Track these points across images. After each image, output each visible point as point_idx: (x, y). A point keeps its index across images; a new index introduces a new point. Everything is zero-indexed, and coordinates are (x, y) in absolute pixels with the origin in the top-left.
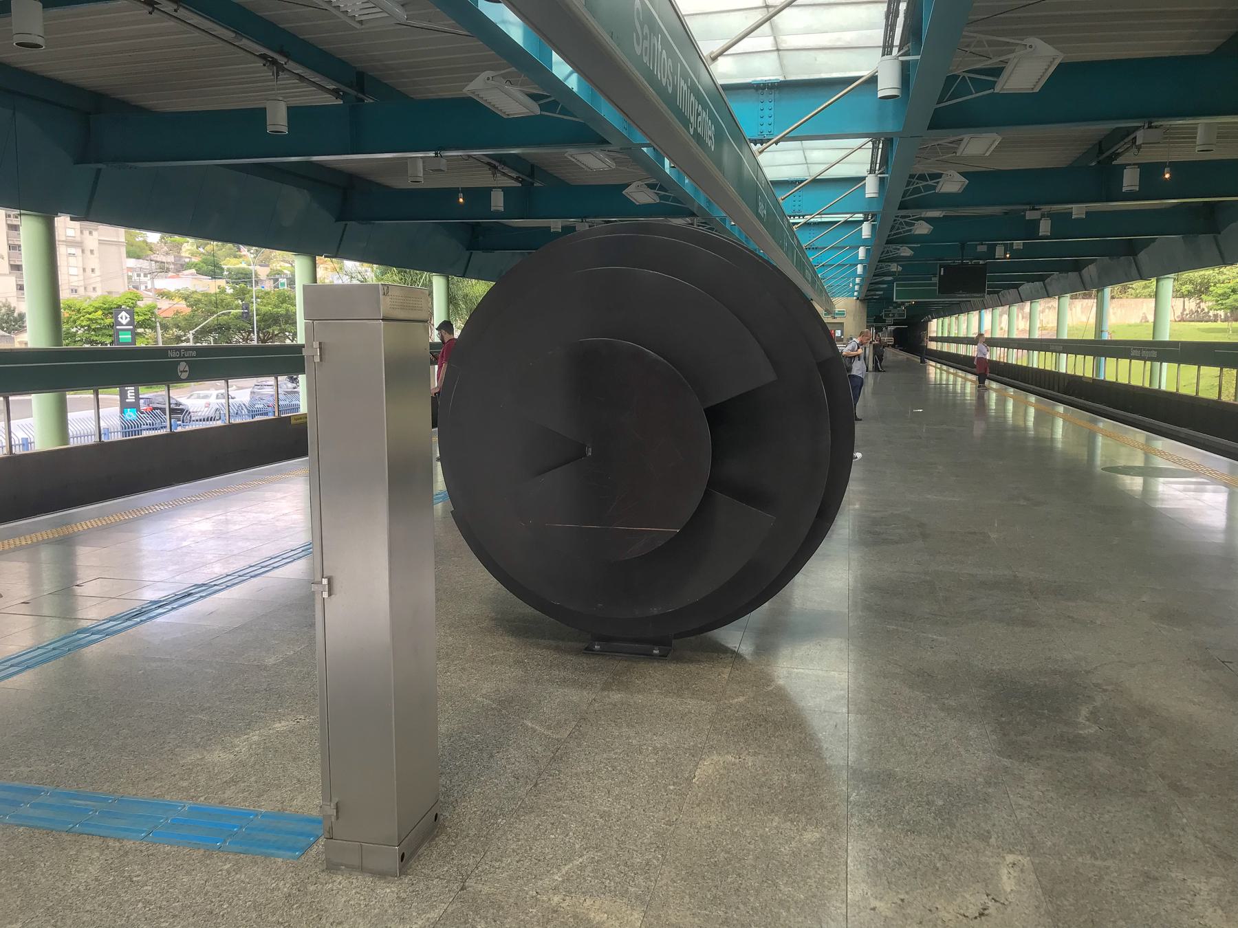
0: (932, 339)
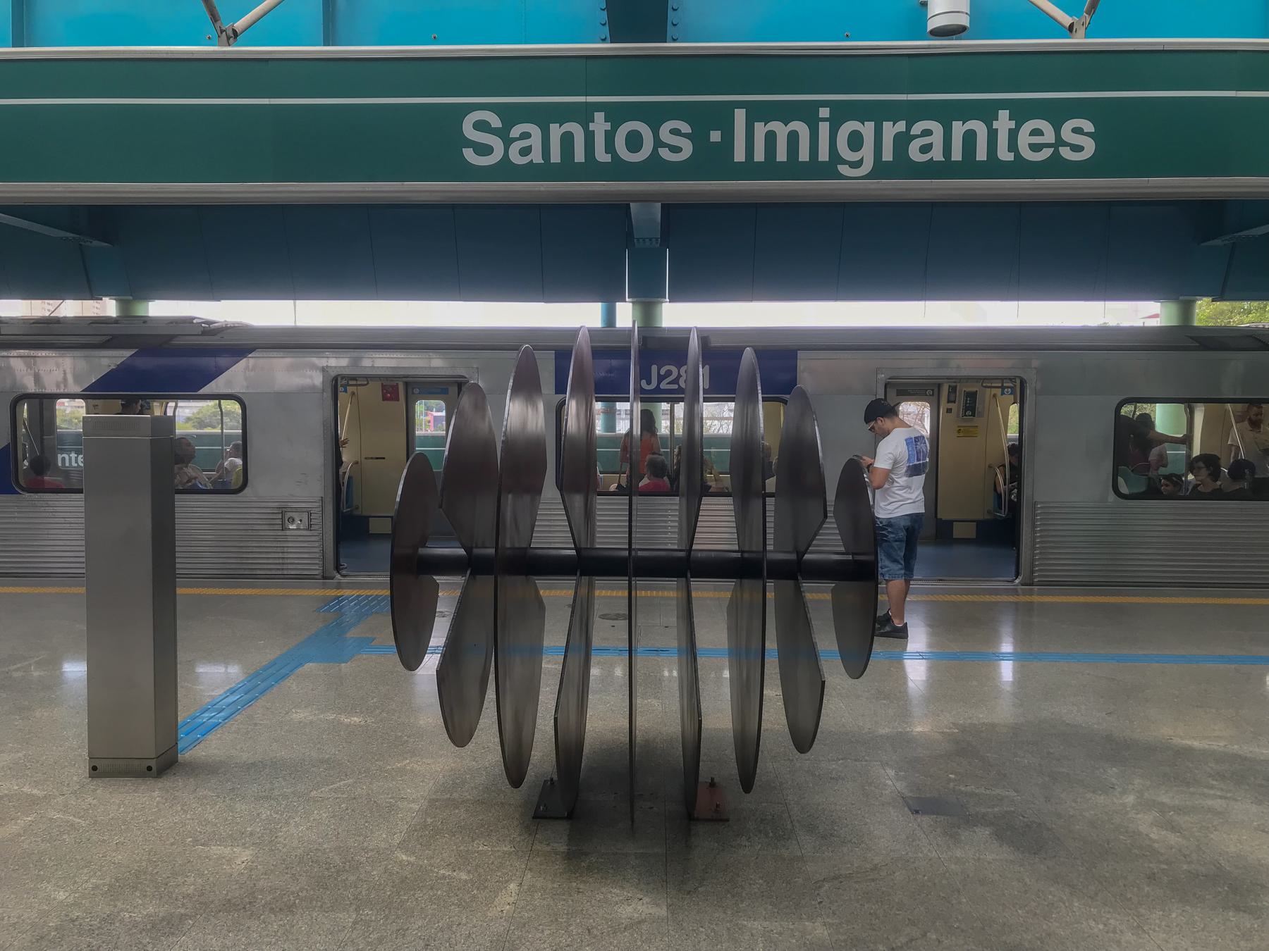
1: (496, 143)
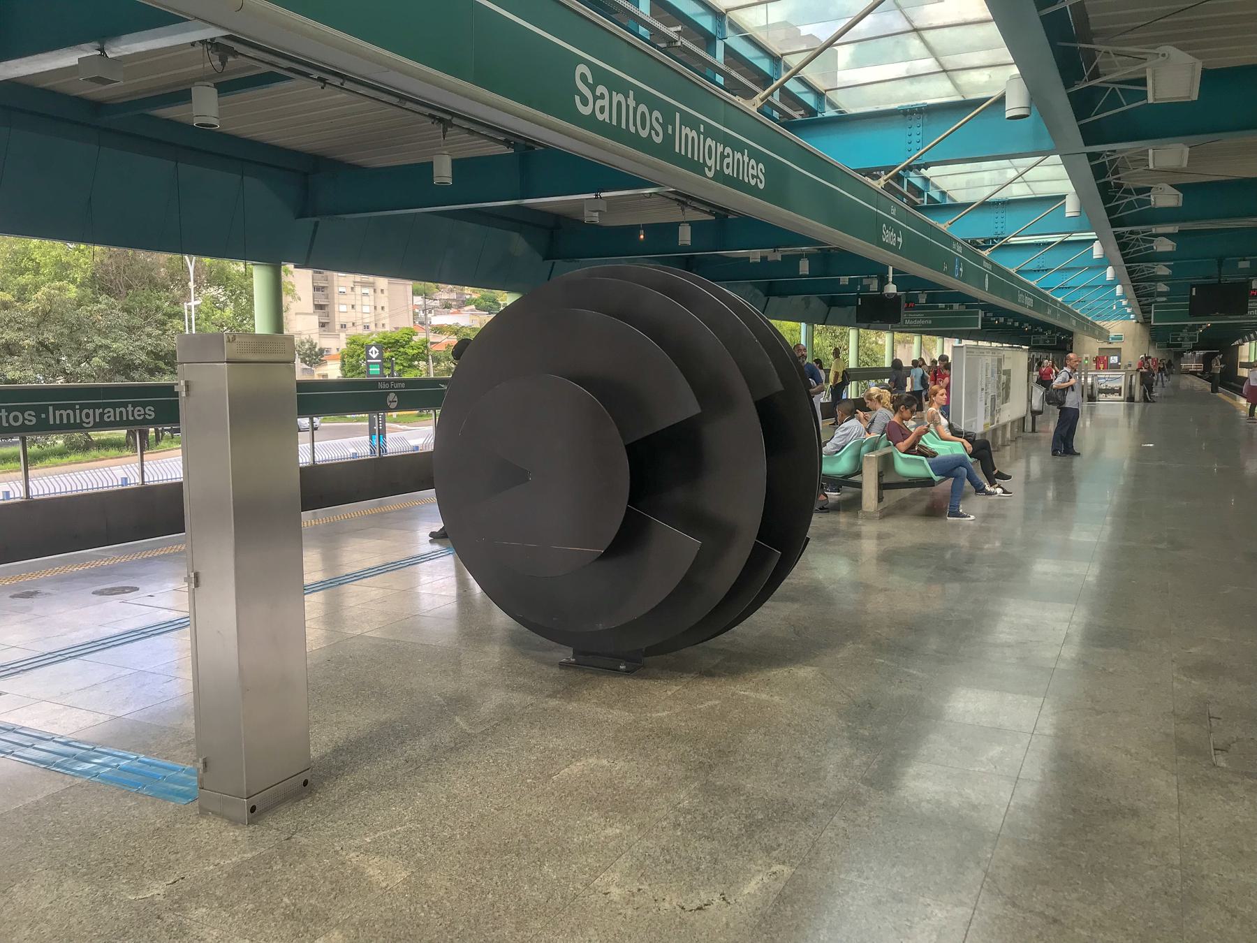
0: (1245, 365)
1: (147, 412)
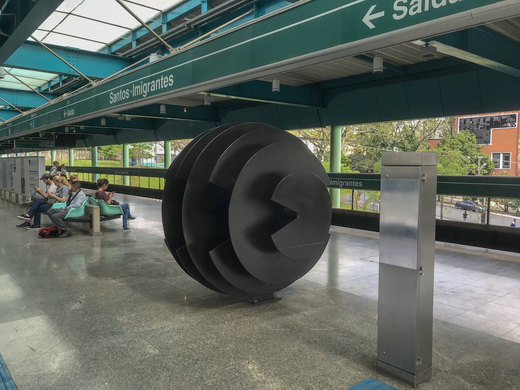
1: (360, 184)
